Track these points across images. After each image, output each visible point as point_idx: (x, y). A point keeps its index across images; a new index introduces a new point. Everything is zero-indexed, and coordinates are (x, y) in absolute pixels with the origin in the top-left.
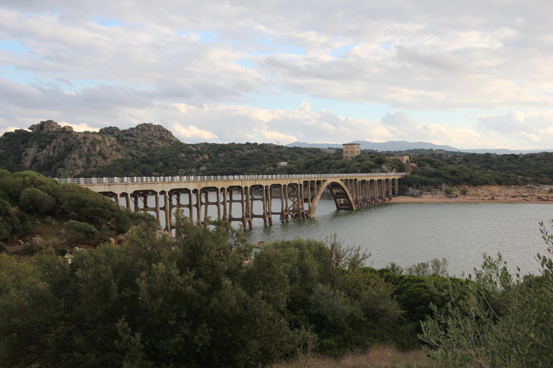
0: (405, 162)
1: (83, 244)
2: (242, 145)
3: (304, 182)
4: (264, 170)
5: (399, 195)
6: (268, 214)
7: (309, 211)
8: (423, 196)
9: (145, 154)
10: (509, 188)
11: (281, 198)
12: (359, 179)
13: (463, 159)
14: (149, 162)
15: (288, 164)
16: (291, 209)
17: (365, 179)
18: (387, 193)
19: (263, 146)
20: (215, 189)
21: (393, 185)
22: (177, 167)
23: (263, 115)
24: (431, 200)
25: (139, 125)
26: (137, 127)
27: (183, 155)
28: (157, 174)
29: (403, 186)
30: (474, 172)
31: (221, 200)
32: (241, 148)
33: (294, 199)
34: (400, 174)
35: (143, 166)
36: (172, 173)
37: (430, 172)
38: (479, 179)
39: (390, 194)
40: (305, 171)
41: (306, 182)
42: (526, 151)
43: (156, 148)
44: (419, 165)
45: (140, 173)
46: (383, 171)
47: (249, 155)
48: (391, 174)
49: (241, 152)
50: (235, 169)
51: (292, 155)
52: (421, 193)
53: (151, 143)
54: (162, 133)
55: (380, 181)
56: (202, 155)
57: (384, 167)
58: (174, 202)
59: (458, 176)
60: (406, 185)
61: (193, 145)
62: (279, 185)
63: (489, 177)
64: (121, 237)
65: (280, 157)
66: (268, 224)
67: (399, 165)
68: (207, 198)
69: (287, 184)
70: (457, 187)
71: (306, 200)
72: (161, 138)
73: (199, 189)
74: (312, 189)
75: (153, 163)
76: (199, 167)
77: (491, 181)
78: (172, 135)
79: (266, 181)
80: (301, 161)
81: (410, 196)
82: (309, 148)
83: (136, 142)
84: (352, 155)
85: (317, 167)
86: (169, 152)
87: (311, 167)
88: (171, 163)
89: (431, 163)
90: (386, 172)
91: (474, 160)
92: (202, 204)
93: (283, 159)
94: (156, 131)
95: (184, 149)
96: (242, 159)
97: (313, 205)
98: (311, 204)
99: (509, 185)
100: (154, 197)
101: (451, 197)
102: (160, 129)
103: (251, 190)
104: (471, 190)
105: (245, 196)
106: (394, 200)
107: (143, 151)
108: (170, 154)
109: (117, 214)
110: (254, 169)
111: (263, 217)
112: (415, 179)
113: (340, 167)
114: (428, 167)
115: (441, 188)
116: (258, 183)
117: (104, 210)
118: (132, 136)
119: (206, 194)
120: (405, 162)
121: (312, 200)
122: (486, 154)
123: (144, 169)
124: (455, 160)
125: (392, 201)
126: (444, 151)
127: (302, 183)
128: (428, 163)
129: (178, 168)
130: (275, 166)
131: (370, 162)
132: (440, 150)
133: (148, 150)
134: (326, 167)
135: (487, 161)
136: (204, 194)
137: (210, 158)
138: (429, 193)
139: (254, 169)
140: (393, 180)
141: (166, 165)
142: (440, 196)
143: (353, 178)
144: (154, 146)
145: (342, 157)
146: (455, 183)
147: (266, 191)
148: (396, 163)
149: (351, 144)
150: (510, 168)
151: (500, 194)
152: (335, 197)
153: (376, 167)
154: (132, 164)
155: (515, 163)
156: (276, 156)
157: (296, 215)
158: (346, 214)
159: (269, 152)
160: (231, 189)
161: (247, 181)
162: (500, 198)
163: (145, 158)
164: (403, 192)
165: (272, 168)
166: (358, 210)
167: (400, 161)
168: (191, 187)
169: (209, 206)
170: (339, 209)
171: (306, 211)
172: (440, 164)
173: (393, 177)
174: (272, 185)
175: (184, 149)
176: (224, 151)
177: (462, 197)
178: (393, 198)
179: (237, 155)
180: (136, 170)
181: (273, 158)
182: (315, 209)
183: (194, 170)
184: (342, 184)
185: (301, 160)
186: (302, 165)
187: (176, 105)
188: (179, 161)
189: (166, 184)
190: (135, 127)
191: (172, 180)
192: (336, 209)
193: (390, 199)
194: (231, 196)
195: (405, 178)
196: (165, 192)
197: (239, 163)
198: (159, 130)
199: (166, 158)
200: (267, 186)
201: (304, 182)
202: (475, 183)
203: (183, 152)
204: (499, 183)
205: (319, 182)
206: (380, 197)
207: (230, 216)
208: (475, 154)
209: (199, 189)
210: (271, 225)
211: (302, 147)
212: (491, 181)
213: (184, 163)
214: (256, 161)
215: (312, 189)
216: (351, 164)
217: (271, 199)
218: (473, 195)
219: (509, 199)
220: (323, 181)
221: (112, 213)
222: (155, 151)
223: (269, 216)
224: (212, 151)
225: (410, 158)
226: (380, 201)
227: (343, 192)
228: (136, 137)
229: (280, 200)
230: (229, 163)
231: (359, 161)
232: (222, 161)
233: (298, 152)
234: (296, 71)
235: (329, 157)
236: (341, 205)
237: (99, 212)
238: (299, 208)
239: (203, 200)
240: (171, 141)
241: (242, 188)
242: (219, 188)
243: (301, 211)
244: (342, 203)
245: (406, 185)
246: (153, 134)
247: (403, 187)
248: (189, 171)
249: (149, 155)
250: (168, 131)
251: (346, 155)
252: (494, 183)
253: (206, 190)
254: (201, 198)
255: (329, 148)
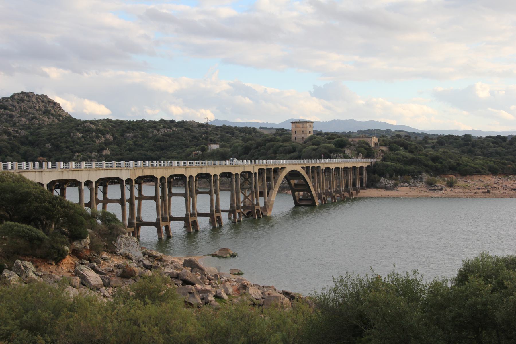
0: (373, 146)
1: (25, 255)
2: (155, 122)
3: (259, 169)
4: (189, 155)
5: (368, 187)
6: (193, 215)
7: (265, 208)
8: (399, 189)
9: (26, 133)
10: (507, 178)
11: (210, 193)
12: (323, 167)
13: (437, 142)
14: (32, 144)
15: (221, 147)
16: (242, 205)
17: (329, 166)
18: (354, 185)
19: (182, 124)
20: (117, 181)
21: (361, 174)
22: (71, 150)
23: (164, 83)
24: (410, 194)
25: (15, 94)
26: (12, 96)
27: (79, 135)
28: (45, 159)
29: (373, 176)
30: (461, 157)
31: (127, 196)
32: (155, 127)
33: (245, 193)
34: (369, 160)
35: (24, 149)
36: (65, 158)
37: (407, 157)
38: (468, 167)
39: (358, 186)
40: (243, 156)
41: (261, 170)
42: (508, 132)
43: (40, 124)
44: (391, 149)
45: (20, 157)
46: (346, 157)
47: (166, 136)
48: (355, 160)
49: (155, 131)
50: (149, 153)
51: (222, 136)
52: (396, 185)
53: (33, 118)
54: (49, 107)
55: (346, 168)
56: (104, 134)
57: (347, 151)
58: (136, 193)
59: (441, 163)
60: (376, 175)
61: (92, 122)
62: (208, 176)
63: (481, 164)
64: (76, 244)
65: (206, 139)
66: (217, 225)
67: (366, 149)
68: (105, 193)
69: (239, 173)
70: (441, 177)
71: (262, 194)
72: (46, 112)
73: (133, 179)
74: (269, 179)
75: (38, 145)
76: (100, 150)
77: (483, 169)
78: (60, 108)
79: (191, 169)
80: (237, 144)
81: (382, 188)
82: (242, 128)
83: (11, 116)
84: (303, 135)
85: (259, 151)
86: (59, 131)
87: (252, 151)
88: (63, 145)
89: (406, 147)
90: (350, 158)
91: (451, 143)
92: (98, 202)
93: (211, 140)
94: (38, 102)
95: (80, 127)
96: (157, 141)
97: (269, 200)
98: (267, 198)
99: (506, 175)
100: (76, 189)
101: (435, 190)
102: (44, 100)
103: (169, 182)
104: (460, 182)
105: (160, 190)
106: (363, 193)
107: (23, 129)
108: (61, 132)
109: (72, 212)
110: (174, 154)
111: (156, 224)
112: (388, 166)
113: (290, 152)
114: (402, 151)
115: (421, 178)
116: (204, 171)
117: (54, 206)
118: (5, 108)
119: (140, 185)
120: (373, 146)
121: (268, 193)
122: (466, 136)
123: (26, 152)
124: (426, 142)
125: (360, 195)
126: (405, 132)
127: (257, 172)
128: (401, 146)
129: (73, 152)
130: (203, 150)
131: (329, 145)
132: (400, 131)
133: (29, 128)
134: (271, 151)
135: (468, 145)
136: (101, 188)
137: (115, 138)
138: (407, 184)
139: (174, 154)
140: (361, 167)
141: (57, 147)
142: (420, 189)
143: (316, 166)
144: (37, 122)
145: (290, 138)
146: (439, 172)
147: (215, 182)
148: (363, 147)
149: (302, 122)
150: (498, 153)
151: (496, 186)
152: (294, 189)
153: (337, 152)
154: (8, 145)
155: (503, 147)
156: (201, 137)
157: (248, 213)
158: (306, 212)
159: (192, 131)
160: (142, 180)
161: (162, 169)
162: (497, 191)
163: (26, 137)
164: (372, 184)
165: (200, 153)
166: (321, 206)
167: (367, 144)
168: (124, 175)
169: (144, 202)
170: (297, 205)
171: (261, 208)
172: (416, 148)
173: (361, 165)
174: (171, 177)
175: (80, 127)
176: (133, 130)
177: (448, 190)
178: (361, 191)
179: (151, 135)
180: (15, 153)
181: (198, 140)
182: (272, 205)
183: (94, 154)
184: (303, 173)
185: (238, 142)
186: (239, 148)
187: (46, 70)
188: (73, 142)
189: (92, 172)
190: (9, 96)
191: (54, 167)
192: (294, 205)
193: (358, 192)
194: (140, 190)
195: (374, 166)
196: (92, 182)
197: (154, 145)
198: (43, 102)
199: (55, 138)
200: (163, 178)
201: (259, 169)
202: (465, 172)
203: (78, 130)
204: (494, 172)
205: (276, 170)
206: (337, 192)
207: (139, 219)
208: (452, 136)
209: (133, 179)
210: (169, 237)
211: (233, 126)
212: (483, 169)
213: (81, 146)
214: (176, 143)
215: (269, 179)
216: (305, 147)
217: (197, 194)
218: (462, 187)
219: (508, 192)
220: (282, 168)
221: (64, 212)
222: (38, 128)
223: (165, 223)
224: (117, 130)
225: (378, 140)
226: (346, 195)
227: (304, 183)
228: (11, 110)
229: (208, 197)
230: (141, 146)
231: (313, 144)
232: (131, 142)
233: (227, 132)
234: (191, 28)
235: (275, 139)
236: (300, 199)
237: (47, 209)
238: (253, 204)
239: (100, 196)
240: (60, 116)
241: (186, 177)
242: (124, 179)
243: (256, 208)
244: (301, 197)
245: (376, 175)
246: (35, 107)
247: (373, 177)
248: (88, 155)
249: (32, 134)
250: (55, 104)
251: (296, 136)
252: (488, 172)
253: (104, 182)
254: (96, 194)
255: (261, 128)
